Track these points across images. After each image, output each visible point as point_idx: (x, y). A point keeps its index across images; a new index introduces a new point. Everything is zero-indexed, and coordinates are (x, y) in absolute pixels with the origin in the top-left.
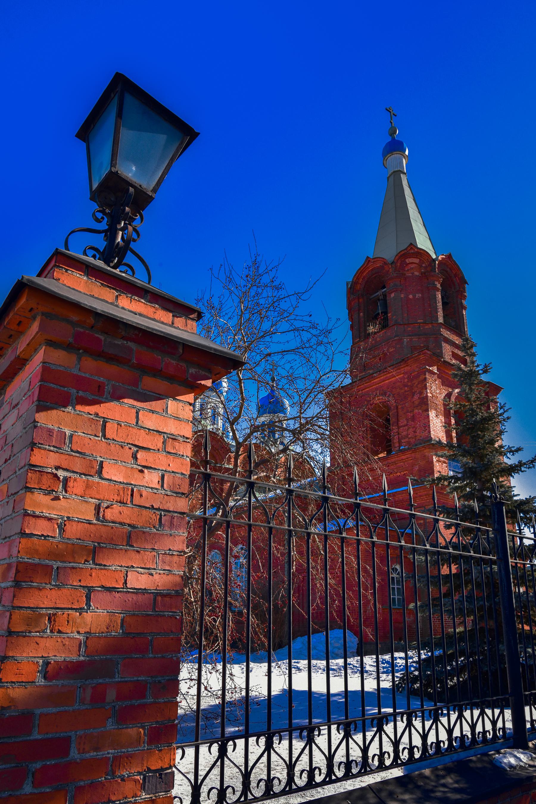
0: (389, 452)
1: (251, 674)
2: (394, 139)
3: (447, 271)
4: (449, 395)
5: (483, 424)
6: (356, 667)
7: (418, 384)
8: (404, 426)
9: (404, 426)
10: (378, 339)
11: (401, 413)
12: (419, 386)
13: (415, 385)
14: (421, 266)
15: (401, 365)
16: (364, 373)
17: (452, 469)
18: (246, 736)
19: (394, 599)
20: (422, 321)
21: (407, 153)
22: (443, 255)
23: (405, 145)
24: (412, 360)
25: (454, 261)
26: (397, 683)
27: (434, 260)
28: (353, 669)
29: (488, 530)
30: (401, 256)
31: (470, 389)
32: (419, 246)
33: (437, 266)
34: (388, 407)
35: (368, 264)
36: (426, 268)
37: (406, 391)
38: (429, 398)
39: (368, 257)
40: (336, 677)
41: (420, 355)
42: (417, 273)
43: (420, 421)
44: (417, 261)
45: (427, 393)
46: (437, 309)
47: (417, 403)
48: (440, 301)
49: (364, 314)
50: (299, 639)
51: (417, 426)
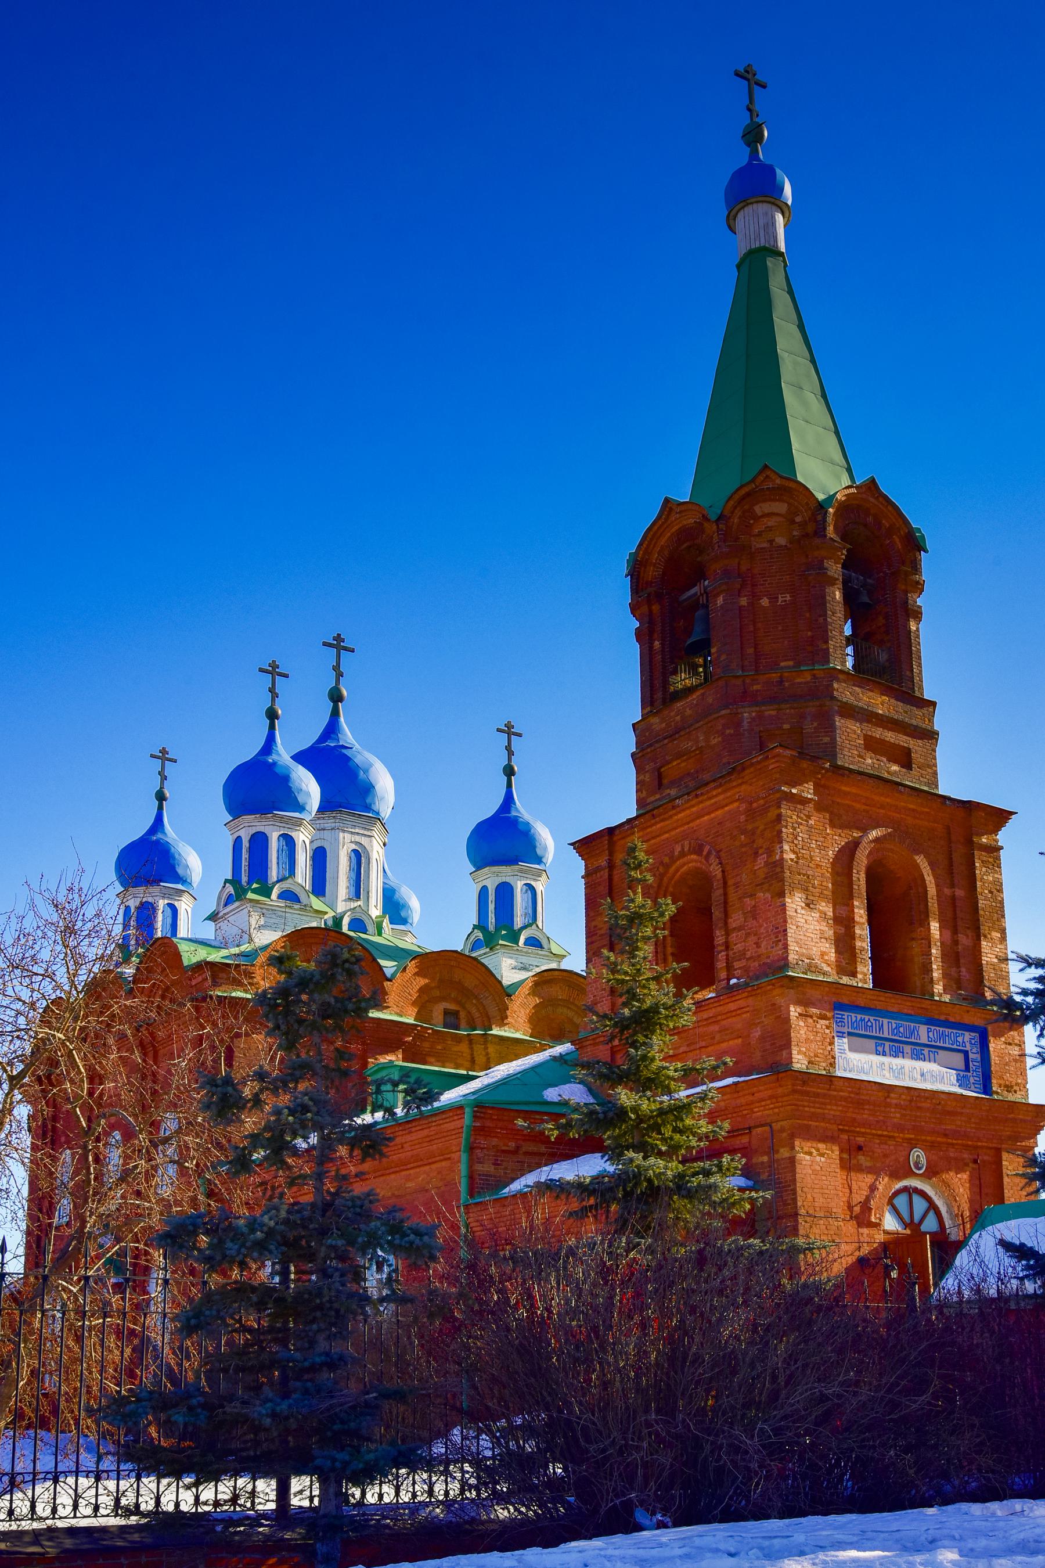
4: (849, 852)
7: (765, 829)
11: (733, 897)
14: (793, 522)
16: (658, 796)
17: (845, 1030)
18: (77, 1473)
23: (778, 171)
24: (752, 769)
25: (886, 498)
30: (743, 499)
34: (706, 879)
36: (803, 525)
42: (781, 541)
44: (781, 508)
45: (782, 852)
51: (762, 930)
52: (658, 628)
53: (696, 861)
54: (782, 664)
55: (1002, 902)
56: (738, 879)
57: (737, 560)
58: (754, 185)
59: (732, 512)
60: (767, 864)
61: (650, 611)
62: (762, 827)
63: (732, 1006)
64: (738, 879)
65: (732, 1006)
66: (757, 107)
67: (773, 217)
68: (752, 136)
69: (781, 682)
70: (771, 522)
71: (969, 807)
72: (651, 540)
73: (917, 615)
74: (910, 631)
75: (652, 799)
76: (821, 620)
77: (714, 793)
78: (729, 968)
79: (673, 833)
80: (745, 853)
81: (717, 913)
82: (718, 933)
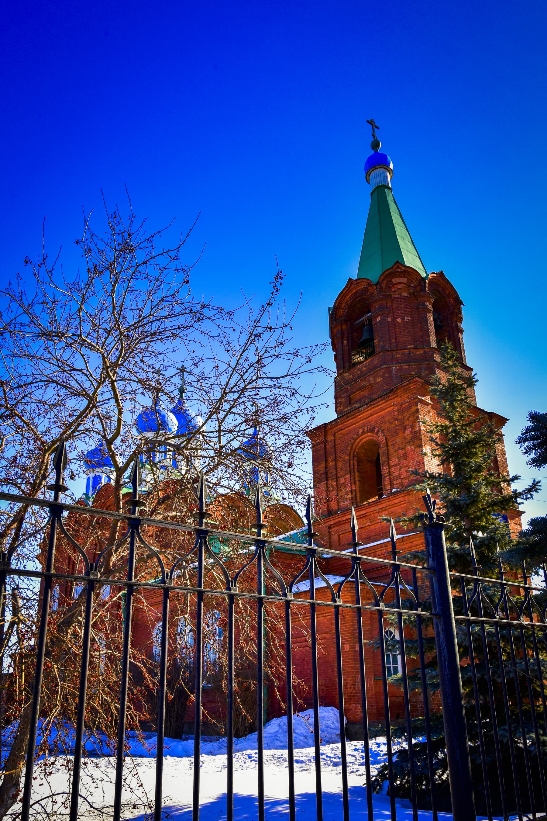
0: (380, 496)
1: (201, 770)
2: (376, 152)
3: (439, 292)
5: (469, 448)
6: (330, 757)
7: (410, 417)
8: (396, 465)
9: (396, 465)
10: (364, 369)
12: (411, 419)
13: (406, 418)
14: (410, 286)
15: (389, 396)
16: (349, 408)
19: (389, 668)
20: (412, 346)
21: (391, 166)
22: (433, 273)
24: (402, 389)
26: (373, 779)
27: (424, 279)
28: (326, 760)
29: (414, 569)
31: (451, 405)
32: (407, 264)
33: (427, 285)
35: (350, 286)
36: (415, 287)
37: (396, 426)
38: (422, 432)
39: (350, 279)
40: (304, 772)
41: (410, 383)
42: (405, 294)
43: (412, 459)
44: (404, 280)
45: (420, 426)
46: (429, 332)
47: (409, 438)
48: (432, 323)
49: (348, 342)
50: (275, 722)
51: (410, 464)
52: (346, 335)
53: (371, 436)
54: (409, 347)
55: (506, 459)
56: (394, 442)
57: (386, 301)
58: (377, 161)
59: (383, 281)
60: (411, 433)
61: (342, 328)
62: (407, 416)
63: (396, 501)
64: (394, 442)
65: (396, 501)
66: (376, 135)
67: (386, 174)
68: (375, 145)
69: (410, 353)
70: (400, 286)
71: (491, 415)
72: (342, 297)
73: (462, 331)
74: (459, 338)
75: (346, 409)
76: (426, 327)
77: (380, 403)
78: (391, 484)
79: (357, 424)
80: (398, 429)
81: (383, 459)
82: (385, 468)
